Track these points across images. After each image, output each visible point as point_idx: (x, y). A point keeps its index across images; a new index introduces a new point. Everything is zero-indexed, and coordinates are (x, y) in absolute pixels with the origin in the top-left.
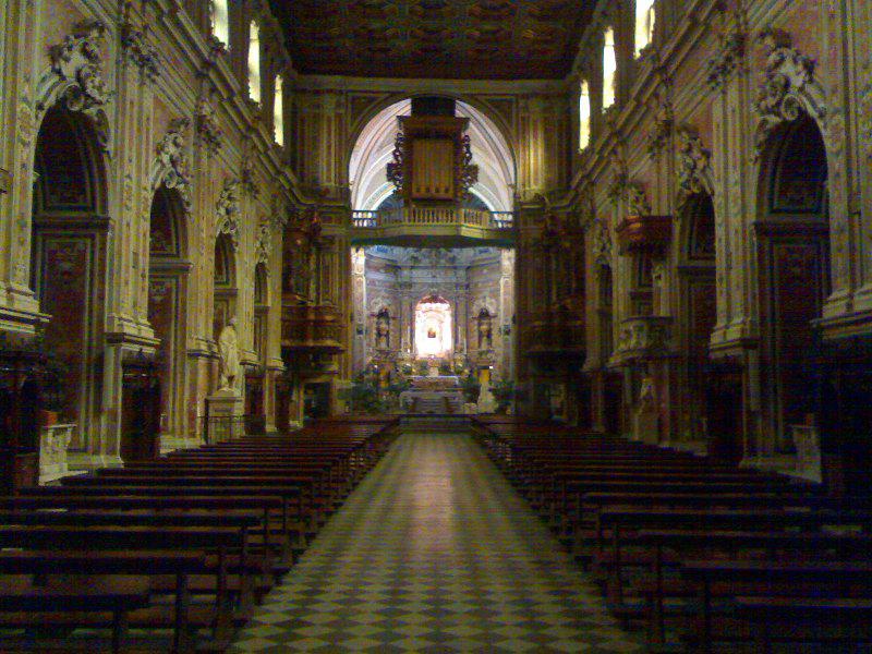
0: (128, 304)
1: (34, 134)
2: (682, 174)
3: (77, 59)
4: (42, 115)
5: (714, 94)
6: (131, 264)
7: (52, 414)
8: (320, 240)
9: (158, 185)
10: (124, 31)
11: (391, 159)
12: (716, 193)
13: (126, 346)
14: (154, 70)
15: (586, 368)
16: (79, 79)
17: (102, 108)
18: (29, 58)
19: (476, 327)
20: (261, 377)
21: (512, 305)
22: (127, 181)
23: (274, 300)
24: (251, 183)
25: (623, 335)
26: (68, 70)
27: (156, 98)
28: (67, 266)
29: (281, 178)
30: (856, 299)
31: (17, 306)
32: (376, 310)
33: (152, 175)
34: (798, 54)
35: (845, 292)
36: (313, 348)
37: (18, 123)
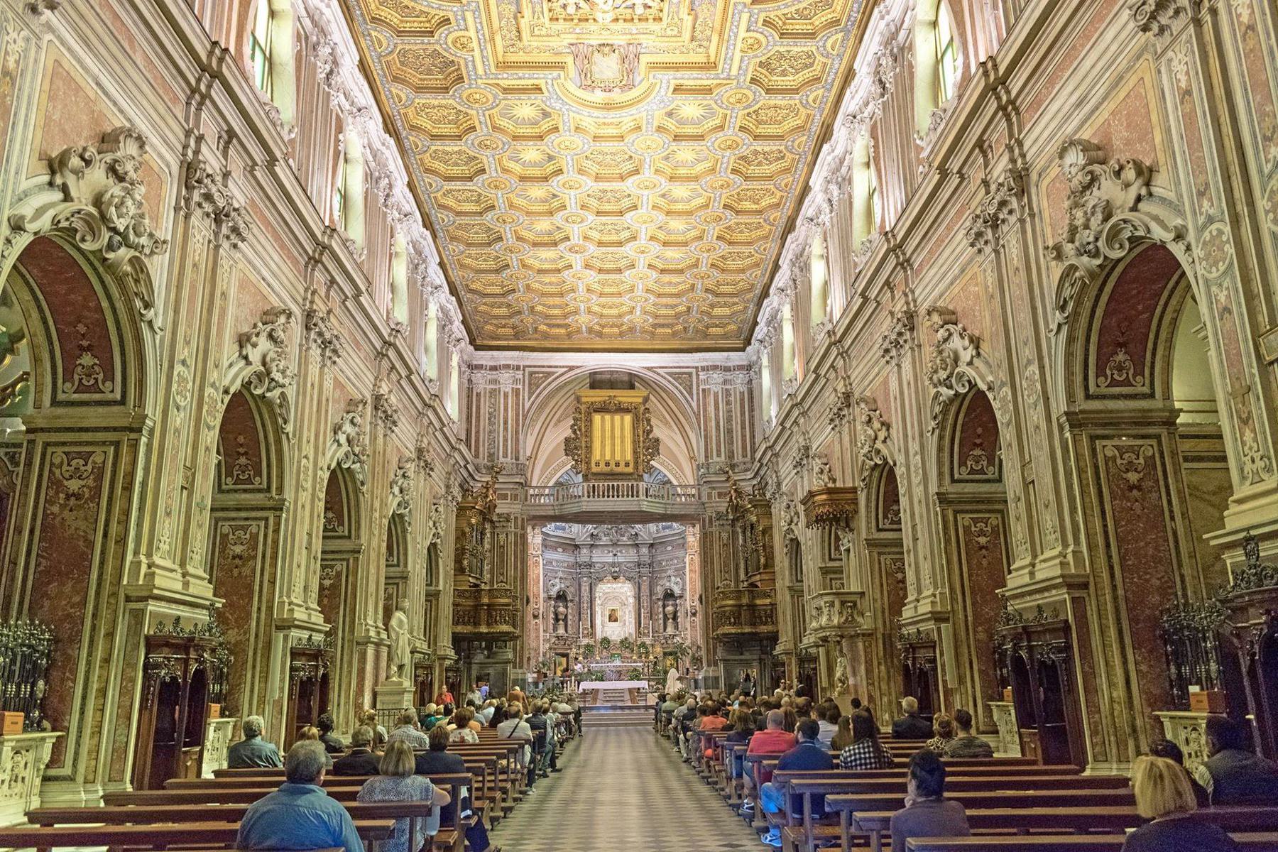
0: (298, 589)
1: (219, 417)
2: (863, 445)
3: (264, 344)
4: (227, 399)
5: (889, 367)
6: (304, 545)
7: (215, 708)
8: (495, 518)
9: (333, 465)
10: (308, 315)
11: (569, 433)
12: (898, 463)
13: (294, 633)
14: (335, 351)
15: (779, 649)
16: (264, 364)
17: (284, 390)
18: (220, 345)
19: (661, 609)
20: (430, 668)
21: (698, 585)
22: (304, 461)
23: (445, 583)
24: (425, 461)
25: (814, 613)
26: (255, 355)
27: (336, 379)
28: (238, 549)
29: (456, 455)
30: (1038, 567)
31: (191, 590)
32: (553, 592)
33: (329, 455)
34: (965, 330)
35: (1028, 561)
36: (487, 633)
37: (205, 408)
